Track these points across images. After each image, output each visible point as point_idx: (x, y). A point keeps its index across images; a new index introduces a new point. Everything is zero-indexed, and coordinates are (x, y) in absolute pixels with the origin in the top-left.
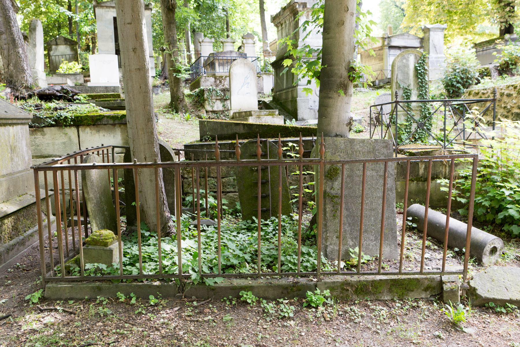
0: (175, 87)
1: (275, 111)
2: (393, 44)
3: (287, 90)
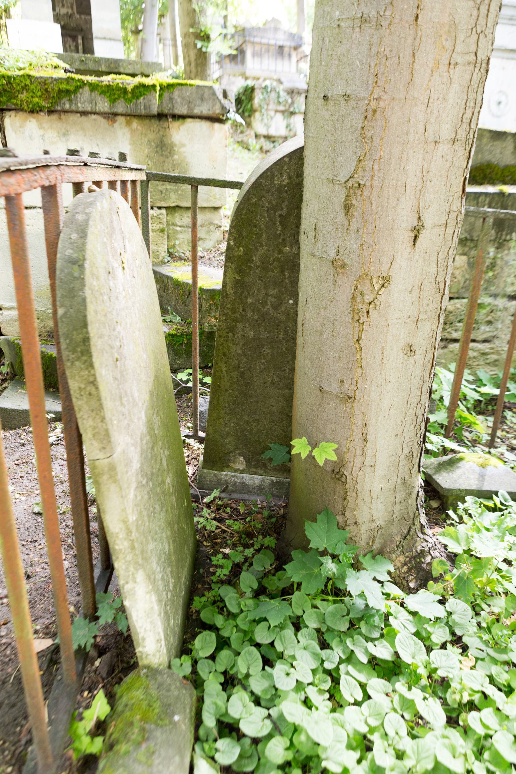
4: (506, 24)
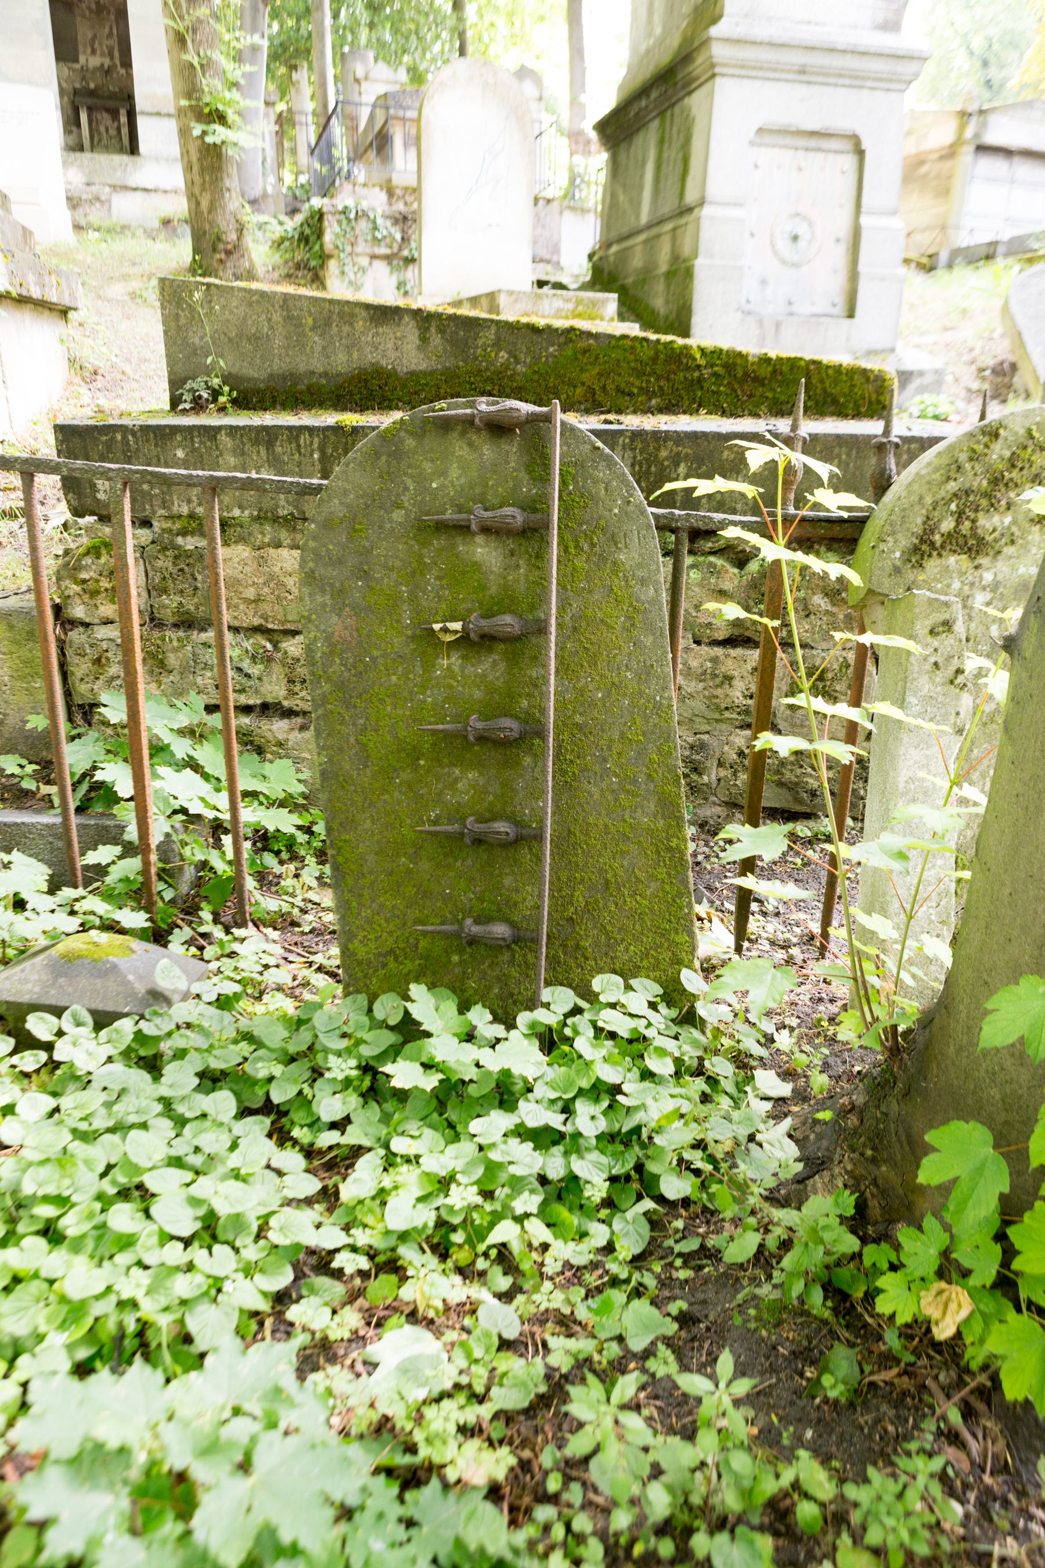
0: (203, 189)
1: (605, 302)
2: (993, 137)
3: (654, 231)
4: (794, 81)
